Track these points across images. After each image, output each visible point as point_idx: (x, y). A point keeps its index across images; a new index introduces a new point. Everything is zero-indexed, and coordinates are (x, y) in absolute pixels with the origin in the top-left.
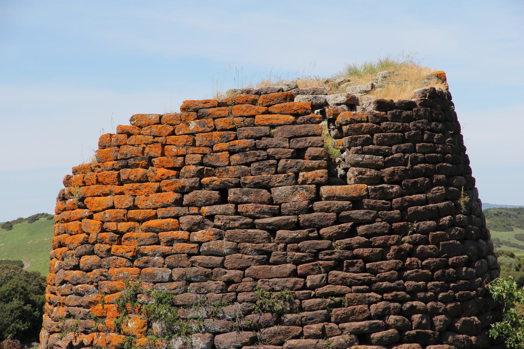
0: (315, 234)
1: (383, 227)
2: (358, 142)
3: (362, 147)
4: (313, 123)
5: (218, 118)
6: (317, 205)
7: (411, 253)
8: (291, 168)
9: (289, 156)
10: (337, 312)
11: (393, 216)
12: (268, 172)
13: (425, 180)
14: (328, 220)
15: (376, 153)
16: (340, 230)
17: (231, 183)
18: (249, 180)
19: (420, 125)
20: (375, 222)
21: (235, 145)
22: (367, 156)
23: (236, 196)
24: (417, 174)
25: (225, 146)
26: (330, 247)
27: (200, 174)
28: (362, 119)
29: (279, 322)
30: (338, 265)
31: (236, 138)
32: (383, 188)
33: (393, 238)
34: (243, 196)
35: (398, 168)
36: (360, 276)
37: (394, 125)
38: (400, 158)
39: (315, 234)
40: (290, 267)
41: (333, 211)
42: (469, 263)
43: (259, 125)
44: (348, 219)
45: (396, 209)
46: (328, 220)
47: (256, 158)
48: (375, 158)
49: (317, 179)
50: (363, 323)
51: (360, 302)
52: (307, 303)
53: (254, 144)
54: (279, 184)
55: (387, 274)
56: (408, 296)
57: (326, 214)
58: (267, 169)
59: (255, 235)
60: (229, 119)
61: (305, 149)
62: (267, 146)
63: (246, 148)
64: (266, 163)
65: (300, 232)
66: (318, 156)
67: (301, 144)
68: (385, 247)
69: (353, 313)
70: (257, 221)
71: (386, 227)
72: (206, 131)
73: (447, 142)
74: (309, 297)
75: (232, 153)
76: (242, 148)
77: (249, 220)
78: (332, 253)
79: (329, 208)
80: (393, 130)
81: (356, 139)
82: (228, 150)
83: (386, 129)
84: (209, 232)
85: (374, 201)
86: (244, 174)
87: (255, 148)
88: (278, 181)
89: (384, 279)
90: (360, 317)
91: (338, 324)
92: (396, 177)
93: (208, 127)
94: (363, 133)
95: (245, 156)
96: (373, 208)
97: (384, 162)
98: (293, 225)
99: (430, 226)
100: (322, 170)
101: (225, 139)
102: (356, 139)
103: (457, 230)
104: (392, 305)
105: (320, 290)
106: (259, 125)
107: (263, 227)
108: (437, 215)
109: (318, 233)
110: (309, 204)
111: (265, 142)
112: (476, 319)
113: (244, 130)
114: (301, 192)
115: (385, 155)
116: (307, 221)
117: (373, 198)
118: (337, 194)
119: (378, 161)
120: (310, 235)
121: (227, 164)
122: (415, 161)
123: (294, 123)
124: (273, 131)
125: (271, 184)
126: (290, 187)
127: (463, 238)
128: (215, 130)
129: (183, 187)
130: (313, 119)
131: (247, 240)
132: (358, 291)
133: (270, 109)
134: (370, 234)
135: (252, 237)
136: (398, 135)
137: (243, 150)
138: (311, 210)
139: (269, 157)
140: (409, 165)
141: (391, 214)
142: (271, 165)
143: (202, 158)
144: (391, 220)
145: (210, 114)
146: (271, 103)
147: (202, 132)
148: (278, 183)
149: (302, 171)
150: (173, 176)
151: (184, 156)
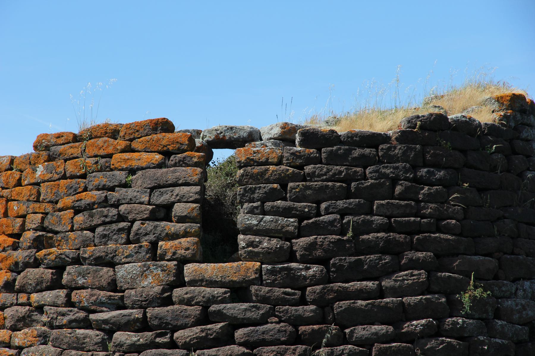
0: (165, 339)
1: (279, 331)
2: (256, 195)
3: (263, 203)
4: (188, 166)
5: (70, 159)
6: (178, 292)
8: (146, 234)
9: (145, 216)
11: (300, 315)
12: (116, 241)
13: (380, 259)
14: (187, 317)
15: (286, 213)
16: (204, 334)
17: (68, 257)
18: (88, 252)
19: (388, 171)
20: (267, 323)
21: (81, 200)
22: (268, 218)
23: (70, 277)
25: (68, 200)
27: (39, 244)
28: (268, 159)
31: (85, 189)
32: (289, 269)
33: (295, 350)
34: (78, 277)
35: (325, 239)
37: (328, 171)
38: (331, 223)
39: (165, 339)
41: (197, 304)
43: (116, 169)
44: (220, 316)
45: (312, 303)
46: (187, 317)
47: (103, 219)
48: (282, 221)
49: (179, 252)
53: (103, 198)
54: (129, 259)
57: (186, 307)
58: (115, 237)
59: (84, 338)
60: (79, 161)
61: (169, 207)
62: (119, 200)
63: (94, 204)
64: (114, 227)
65: (143, 335)
66: (186, 216)
67: (163, 197)
70: (92, 317)
71: (285, 331)
72: (53, 179)
73: (452, 200)
75: (77, 211)
76: (88, 204)
77: (82, 314)
79: (191, 298)
80: (325, 177)
81: (253, 191)
82: (73, 208)
83: (312, 176)
84: (32, 332)
85: (267, 289)
86: (86, 244)
87: (105, 203)
88: (126, 254)
92: (319, 253)
93: (56, 173)
94: (268, 181)
95: (89, 216)
96: (264, 300)
97: (299, 228)
98: (138, 324)
99: (376, 334)
100: (189, 239)
101: (72, 190)
102: (253, 191)
103: (443, 342)
106: (116, 169)
107: (99, 326)
108: (398, 316)
109: (172, 337)
110: (164, 291)
111: (114, 196)
113: (94, 177)
114: (155, 272)
115: (302, 217)
116: (156, 318)
117: (267, 285)
118: (207, 276)
119: (288, 226)
120: (158, 340)
121: (69, 228)
122: (359, 230)
123: (160, 166)
124: (131, 178)
125: (117, 259)
126: (140, 264)
128: (64, 177)
129: (16, 264)
130: (188, 159)
131: (75, 345)
133: (135, 145)
134: (254, 342)
135: (81, 342)
136: (334, 186)
137: (90, 207)
138: (168, 301)
139: (121, 218)
140: (350, 234)
141: (296, 311)
142: (120, 230)
143: (43, 219)
144: (297, 321)
145: (60, 154)
146: (136, 135)
147: (48, 181)
148: (126, 257)
149: (163, 240)
150: (8, 247)
151: (24, 216)
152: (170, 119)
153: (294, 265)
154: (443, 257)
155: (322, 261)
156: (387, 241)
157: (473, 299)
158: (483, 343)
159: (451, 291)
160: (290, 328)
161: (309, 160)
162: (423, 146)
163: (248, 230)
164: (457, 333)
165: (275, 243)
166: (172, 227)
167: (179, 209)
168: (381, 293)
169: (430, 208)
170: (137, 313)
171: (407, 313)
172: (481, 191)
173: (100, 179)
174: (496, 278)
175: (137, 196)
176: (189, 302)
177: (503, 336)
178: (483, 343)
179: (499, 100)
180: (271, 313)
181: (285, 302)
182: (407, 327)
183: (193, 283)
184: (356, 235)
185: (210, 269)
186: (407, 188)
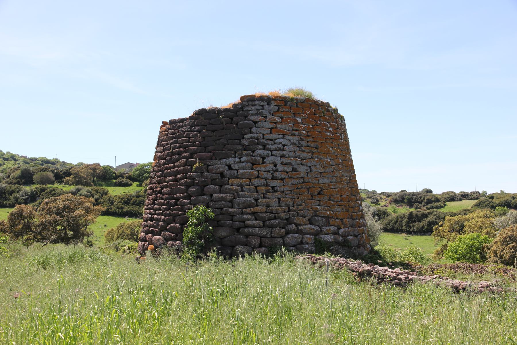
155: (165, 159)
164: (191, 178)
168: (174, 167)
186: (187, 134)
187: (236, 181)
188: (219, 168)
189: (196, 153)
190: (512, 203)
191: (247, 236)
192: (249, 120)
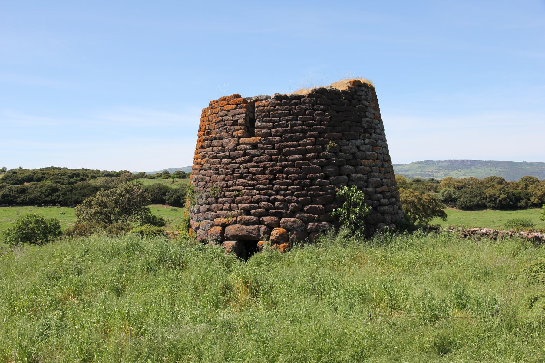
6: (238, 147)
7: (281, 171)
10: (237, 199)
15: (269, 121)
24: (296, 131)
25: (214, 121)
26: (239, 168)
29: (217, 202)
30: (242, 176)
32: (269, 139)
36: (249, 182)
38: (283, 124)
40: (223, 176)
42: (321, 178)
44: (249, 154)
45: (277, 149)
48: (268, 124)
50: (247, 205)
51: (247, 195)
52: (227, 194)
55: (262, 182)
56: (274, 193)
61: (237, 121)
64: (223, 128)
67: (235, 119)
68: (265, 168)
69: (243, 200)
74: (228, 191)
78: (239, 171)
81: (260, 115)
83: (278, 109)
87: (222, 121)
89: (261, 184)
90: (246, 202)
91: (237, 204)
92: (279, 133)
94: (265, 112)
96: (262, 148)
102: (260, 115)
104: (263, 197)
105: (232, 188)
110: (234, 147)
111: (224, 118)
112: (321, 206)
115: (274, 122)
122: (292, 126)
123: (235, 108)
127: (322, 166)
132: (247, 189)
133: (230, 103)
137: (218, 122)
138: (236, 150)
144: (271, 155)
152: (318, 87)
153: (271, 137)
154: (321, 133)
155: (280, 136)
156: (302, 129)
157: (331, 146)
158: (334, 160)
159: (323, 144)
160: (269, 157)
161: (277, 105)
162: (317, 98)
163: (258, 127)
164: (324, 157)
165: (265, 131)
166: (237, 127)
167: (240, 122)
168: (299, 145)
169: (318, 118)
170: (227, 154)
171: (308, 151)
172: (337, 112)
173: (221, 113)
174: (341, 139)
175: (229, 119)
176: (240, 150)
177: (342, 157)
178: (334, 160)
179: (350, 82)
180: (264, 152)
181: (268, 149)
182: (307, 156)
183: (242, 144)
184: (292, 127)
185: (247, 140)
186: (310, 112)
187: (367, 162)
188: (351, 149)
189: (326, 133)
190: (34, 178)
191: (382, 214)
192: (363, 104)
